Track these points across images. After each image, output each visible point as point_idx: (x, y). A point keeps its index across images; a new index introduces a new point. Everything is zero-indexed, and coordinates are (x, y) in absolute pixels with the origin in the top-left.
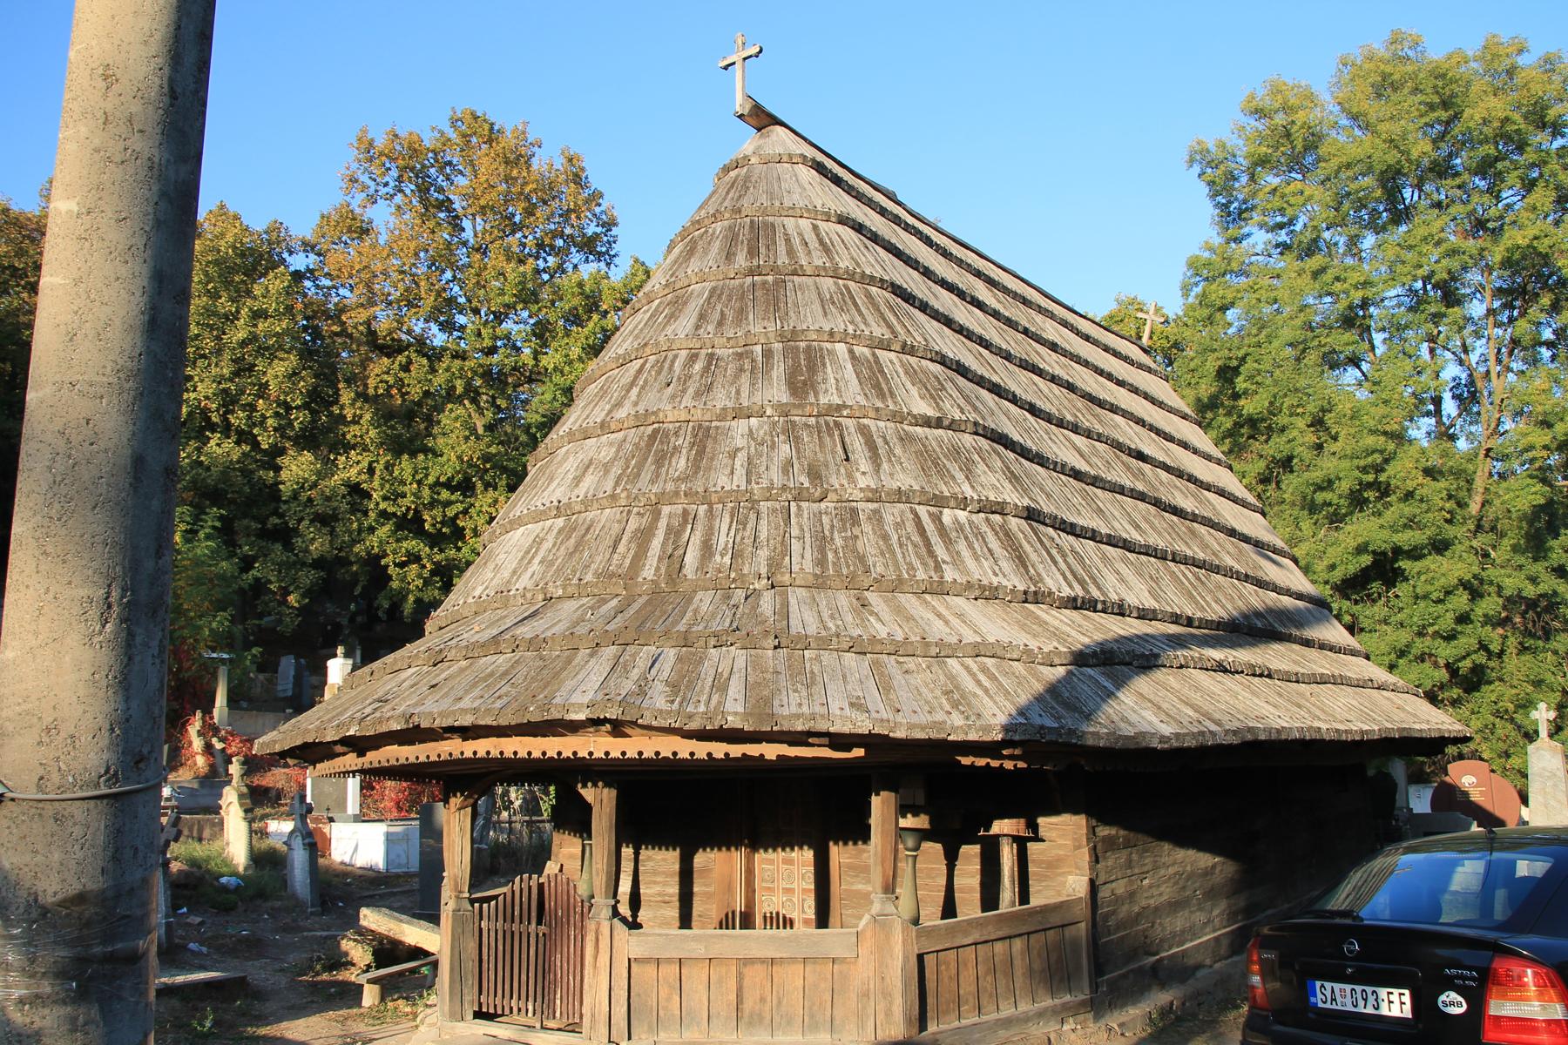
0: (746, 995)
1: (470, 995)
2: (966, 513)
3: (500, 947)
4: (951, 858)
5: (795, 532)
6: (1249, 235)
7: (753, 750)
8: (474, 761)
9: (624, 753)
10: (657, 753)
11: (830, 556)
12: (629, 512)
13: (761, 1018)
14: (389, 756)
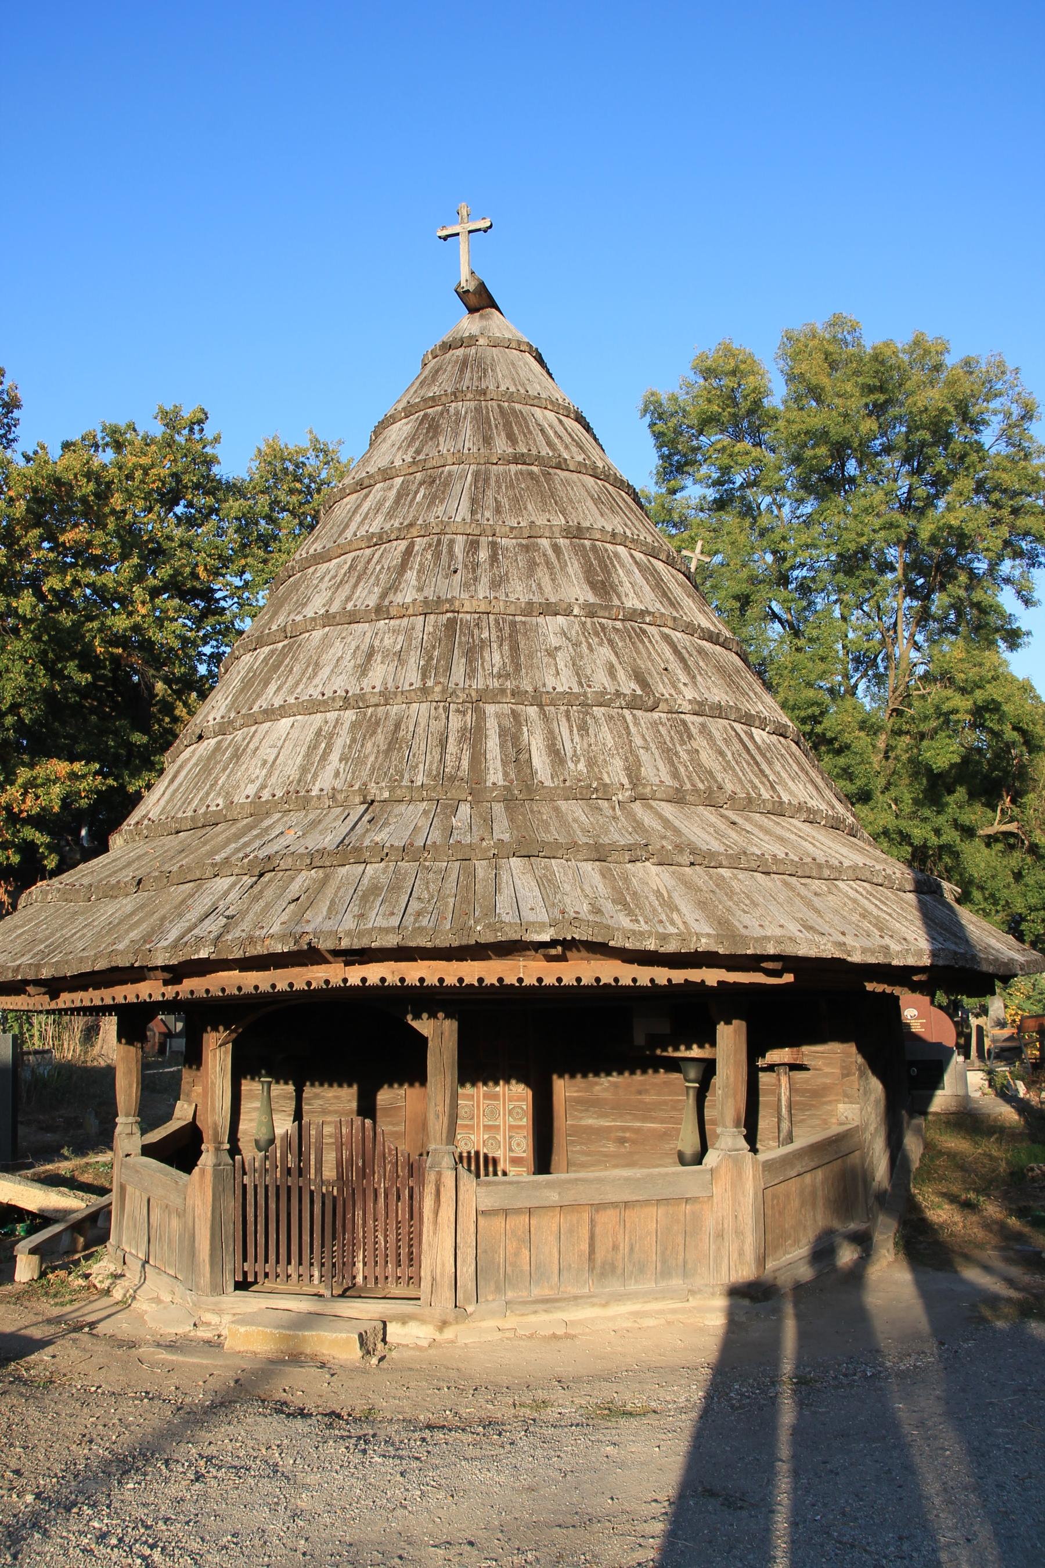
0: (598, 1245)
1: (230, 1262)
2: (764, 734)
3: (272, 1206)
5: (638, 741)
6: (683, 488)
7: (695, 975)
8: (364, 990)
9: (559, 980)
10: (520, 980)
11: (682, 770)
12: (447, 710)
13: (613, 1268)
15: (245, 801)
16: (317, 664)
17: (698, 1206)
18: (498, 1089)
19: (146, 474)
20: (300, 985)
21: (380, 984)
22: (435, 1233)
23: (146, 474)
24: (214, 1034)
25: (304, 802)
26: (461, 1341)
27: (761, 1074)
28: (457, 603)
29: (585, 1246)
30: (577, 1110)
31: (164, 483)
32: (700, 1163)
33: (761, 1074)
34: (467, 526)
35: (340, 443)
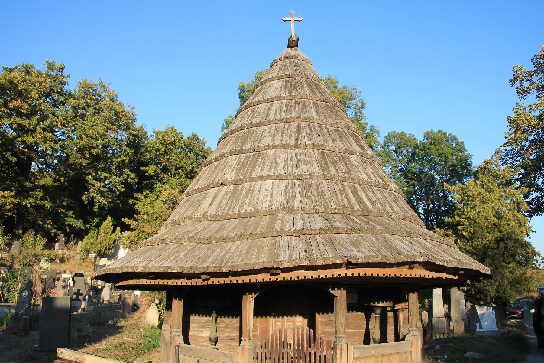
4: (368, 318)
10: (305, 277)
14: (298, 275)
16: (276, 163)
19: (40, 85)
20: (329, 276)
23: (40, 85)
24: (251, 296)
25: (292, 211)
27: (388, 313)
31: (47, 90)
33: (388, 313)
35: (110, 84)
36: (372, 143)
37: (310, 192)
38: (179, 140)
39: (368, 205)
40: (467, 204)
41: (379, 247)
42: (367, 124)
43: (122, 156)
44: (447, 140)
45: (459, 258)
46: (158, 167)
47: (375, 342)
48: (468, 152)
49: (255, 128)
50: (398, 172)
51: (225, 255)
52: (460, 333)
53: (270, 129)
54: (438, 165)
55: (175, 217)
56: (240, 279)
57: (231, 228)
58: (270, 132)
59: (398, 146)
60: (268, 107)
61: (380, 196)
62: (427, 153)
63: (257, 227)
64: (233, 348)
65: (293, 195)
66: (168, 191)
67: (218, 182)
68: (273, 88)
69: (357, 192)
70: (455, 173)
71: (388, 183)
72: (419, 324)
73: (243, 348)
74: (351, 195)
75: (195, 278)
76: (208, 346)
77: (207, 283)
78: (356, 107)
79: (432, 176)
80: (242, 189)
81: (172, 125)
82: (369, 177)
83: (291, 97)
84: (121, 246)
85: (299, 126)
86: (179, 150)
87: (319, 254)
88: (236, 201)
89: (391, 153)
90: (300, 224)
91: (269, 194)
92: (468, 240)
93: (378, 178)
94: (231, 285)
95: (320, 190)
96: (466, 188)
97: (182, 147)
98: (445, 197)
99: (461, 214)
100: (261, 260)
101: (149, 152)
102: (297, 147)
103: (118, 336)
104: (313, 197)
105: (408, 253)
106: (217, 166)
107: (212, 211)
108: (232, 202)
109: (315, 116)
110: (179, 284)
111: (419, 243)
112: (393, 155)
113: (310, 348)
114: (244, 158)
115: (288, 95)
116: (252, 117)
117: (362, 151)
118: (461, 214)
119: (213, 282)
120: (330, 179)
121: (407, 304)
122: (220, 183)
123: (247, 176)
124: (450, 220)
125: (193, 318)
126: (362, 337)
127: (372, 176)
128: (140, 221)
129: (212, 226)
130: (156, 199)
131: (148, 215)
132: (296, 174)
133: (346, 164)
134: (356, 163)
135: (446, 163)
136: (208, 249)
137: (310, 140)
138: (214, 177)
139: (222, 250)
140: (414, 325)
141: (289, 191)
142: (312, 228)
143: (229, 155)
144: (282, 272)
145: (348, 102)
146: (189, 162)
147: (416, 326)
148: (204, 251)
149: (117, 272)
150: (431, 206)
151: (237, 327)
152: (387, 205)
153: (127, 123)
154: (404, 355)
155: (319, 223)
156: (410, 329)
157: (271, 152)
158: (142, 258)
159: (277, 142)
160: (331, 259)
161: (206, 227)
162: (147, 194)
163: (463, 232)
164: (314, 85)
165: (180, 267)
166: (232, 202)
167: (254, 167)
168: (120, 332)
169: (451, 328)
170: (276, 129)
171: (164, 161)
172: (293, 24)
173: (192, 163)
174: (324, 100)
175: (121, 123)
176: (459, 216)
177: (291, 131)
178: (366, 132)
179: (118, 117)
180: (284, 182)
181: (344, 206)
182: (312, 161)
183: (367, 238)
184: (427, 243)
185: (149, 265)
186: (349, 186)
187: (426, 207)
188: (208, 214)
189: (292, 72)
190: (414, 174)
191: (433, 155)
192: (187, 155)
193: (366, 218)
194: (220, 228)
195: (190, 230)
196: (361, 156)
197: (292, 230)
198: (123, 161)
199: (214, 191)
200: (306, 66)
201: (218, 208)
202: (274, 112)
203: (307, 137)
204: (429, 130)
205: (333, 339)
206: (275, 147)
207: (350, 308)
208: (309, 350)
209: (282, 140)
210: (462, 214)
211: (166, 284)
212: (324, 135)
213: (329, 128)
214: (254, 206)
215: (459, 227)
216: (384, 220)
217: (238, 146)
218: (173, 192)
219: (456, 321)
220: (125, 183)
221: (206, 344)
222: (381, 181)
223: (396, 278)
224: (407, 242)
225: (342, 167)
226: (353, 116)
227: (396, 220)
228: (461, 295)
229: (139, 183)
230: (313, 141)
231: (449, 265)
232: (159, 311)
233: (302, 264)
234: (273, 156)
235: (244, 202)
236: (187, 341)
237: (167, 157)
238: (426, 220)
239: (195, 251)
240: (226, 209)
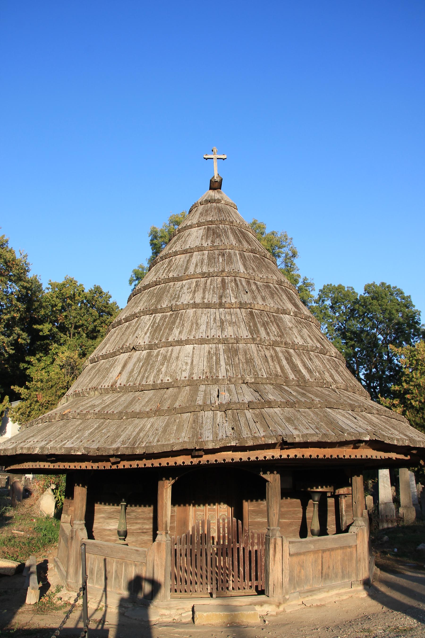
4: (304, 506)
14: (225, 457)
15: (184, 379)
16: (197, 324)
17: (352, 549)
18: (215, 507)
20: (261, 458)
21: (294, 457)
22: (274, 565)
24: (168, 481)
25: (216, 381)
26: (288, 611)
27: (328, 499)
28: (253, 305)
29: (320, 567)
30: (253, 515)
32: (348, 532)
33: (328, 499)
34: (245, 275)
36: (305, 298)
37: (236, 359)
38: (80, 293)
39: (304, 373)
40: (417, 369)
41: (318, 423)
42: (299, 276)
43: (12, 313)
44: (392, 294)
45: (411, 435)
46: (54, 325)
47: (313, 534)
48: (416, 308)
49: (172, 284)
50: (336, 331)
51: (138, 434)
52: (411, 522)
53: (190, 284)
54: (381, 322)
55: (77, 387)
56: (156, 463)
57: (145, 401)
58: (190, 288)
59: (335, 301)
60: (187, 258)
61: (318, 363)
62: (368, 309)
63: (176, 401)
64: (146, 543)
65: (218, 362)
66: (66, 354)
67: (129, 347)
68: (192, 237)
69: (291, 358)
70: (400, 332)
71: (327, 348)
72: (365, 512)
73: (159, 544)
74: (284, 362)
75: (102, 461)
76: (115, 540)
77: (117, 466)
78: (286, 256)
79: (375, 335)
80: (157, 355)
81: (71, 276)
82: (305, 341)
83: (214, 247)
84: (10, 419)
85: (223, 281)
86: (79, 305)
87: (249, 433)
88: (150, 369)
89: (326, 309)
90: (225, 398)
91: (188, 361)
92: (418, 411)
93: (315, 341)
94: (145, 470)
95: (248, 356)
96: (415, 351)
97: (82, 302)
98: (390, 360)
99: (410, 381)
100: (181, 440)
101: (44, 307)
102: (221, 305)
103: (6, 528)
104: (241, 365)
105: (352, 430)
106: (128, 327)
107: (122, 380)
108: (146, 370)
109: (242, 269)
110: (83, 467)
111: (364, 418)
112: (330, 312)
113: (238, 542)
114: (159, 318)
115: (210, 244)
116: (169, 270)
117: (296, 310)
118: (410, 381)
119: (124, 466)
120: (260, 343)
121: (350, 488)
122: (131, 347)
123: (163, 340)
124: (397, 388)
125: (98, 507)
126: (297, 528)
127: (309, 340)
128: (32, 390)
129: (123, 399)
130: (52, 363)
131: (42, 381)
132: (221, 337)
133: (278, 325)
134: (290, 325)
135: (390, 320)
136: (118, 427)
137: (236, 298)
138: (124, 340)
139: (135, 427)
140: (359, 514)
141: (212, 358)
142: (240, 401)
143: (142, 314)
144: (205, 454)
145: (277, 250)
146: (90, 319)
147: (362, 515)
148: (113, 428)
149: (9, 453)
150: (374, 370)
151: (150, 518)
152: (326, 373)
153: (18, 274)
154: (349, 550)
155: (248, 396)
156: (355, 519)
157: (191, 311)
158: (39, 437)
159: (198, 300)
160: (263, 439)
161: (115, 400)
162: (41, 357)
163: (412, 401)
164: (241, 234)
165: (85, 448)
166: (146, 370)
167: (171, 329)
168: (8, 524)
169: (400, 514)
170: (197, 285)
171: (61, 318)
172: (215, 163)
173: (95, 321)
174: (252, 251)
175: (11, 274)
176: (407, 383)
177: (214, 287)
178: (298, 285)
179: (8, 266)
180: (206, 347)
181: (277, 375)
182: (239, 322)
183: (305, 412)
184: (373, 418)
185: (49, 446)
186: (282, 352)
187: (368, 372)
188: (118, 385)
189: (215, 218)
190: (354, 333)
191: (375, 311)
192: (88, 311)
193: (303, 389)
194: (132, 401)
195: (96, 404)
196: (296, 316)
197: (217, 404)
198: (13, 318)
199: (123, 357)
200: (231, 211)
201: (129, 377)
202: (195, 264)
203: (233, 294)
204: (371, 282)
205: (266, 531)
206: (195, 306)
207: (285, 493)
208: (237, 545)
209: (203, 298)
210: (411, 380)
211: (68, 468)
212: (253, 292)
213: (258, 283)
214: (171, 375)
215: (408, 396)
216: (324, 391)
217: (152, 305)
218: (73, 354)
219: (406, 507)
220: (15, 344)
221: (114, 538)
222: (319, 345)
223: (338, 460)
224: (351, 417)
225: (274, 329)
226: (283, 266)
227: (337, 390)
228: (411, 476)
229: (31, 344)
230: (240, 299)
231: (400, 444)
232: (55, 497)
233: (229, 445)
234: (193, 317)
235: (159, 371)
236: (91, 536)
237: (65, 314)
238: (368, 387)
239: (103, 429)
240: (139, 378)
